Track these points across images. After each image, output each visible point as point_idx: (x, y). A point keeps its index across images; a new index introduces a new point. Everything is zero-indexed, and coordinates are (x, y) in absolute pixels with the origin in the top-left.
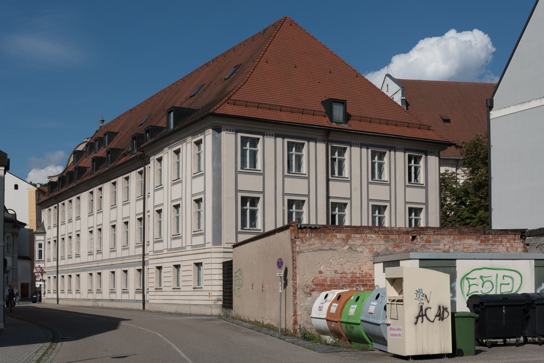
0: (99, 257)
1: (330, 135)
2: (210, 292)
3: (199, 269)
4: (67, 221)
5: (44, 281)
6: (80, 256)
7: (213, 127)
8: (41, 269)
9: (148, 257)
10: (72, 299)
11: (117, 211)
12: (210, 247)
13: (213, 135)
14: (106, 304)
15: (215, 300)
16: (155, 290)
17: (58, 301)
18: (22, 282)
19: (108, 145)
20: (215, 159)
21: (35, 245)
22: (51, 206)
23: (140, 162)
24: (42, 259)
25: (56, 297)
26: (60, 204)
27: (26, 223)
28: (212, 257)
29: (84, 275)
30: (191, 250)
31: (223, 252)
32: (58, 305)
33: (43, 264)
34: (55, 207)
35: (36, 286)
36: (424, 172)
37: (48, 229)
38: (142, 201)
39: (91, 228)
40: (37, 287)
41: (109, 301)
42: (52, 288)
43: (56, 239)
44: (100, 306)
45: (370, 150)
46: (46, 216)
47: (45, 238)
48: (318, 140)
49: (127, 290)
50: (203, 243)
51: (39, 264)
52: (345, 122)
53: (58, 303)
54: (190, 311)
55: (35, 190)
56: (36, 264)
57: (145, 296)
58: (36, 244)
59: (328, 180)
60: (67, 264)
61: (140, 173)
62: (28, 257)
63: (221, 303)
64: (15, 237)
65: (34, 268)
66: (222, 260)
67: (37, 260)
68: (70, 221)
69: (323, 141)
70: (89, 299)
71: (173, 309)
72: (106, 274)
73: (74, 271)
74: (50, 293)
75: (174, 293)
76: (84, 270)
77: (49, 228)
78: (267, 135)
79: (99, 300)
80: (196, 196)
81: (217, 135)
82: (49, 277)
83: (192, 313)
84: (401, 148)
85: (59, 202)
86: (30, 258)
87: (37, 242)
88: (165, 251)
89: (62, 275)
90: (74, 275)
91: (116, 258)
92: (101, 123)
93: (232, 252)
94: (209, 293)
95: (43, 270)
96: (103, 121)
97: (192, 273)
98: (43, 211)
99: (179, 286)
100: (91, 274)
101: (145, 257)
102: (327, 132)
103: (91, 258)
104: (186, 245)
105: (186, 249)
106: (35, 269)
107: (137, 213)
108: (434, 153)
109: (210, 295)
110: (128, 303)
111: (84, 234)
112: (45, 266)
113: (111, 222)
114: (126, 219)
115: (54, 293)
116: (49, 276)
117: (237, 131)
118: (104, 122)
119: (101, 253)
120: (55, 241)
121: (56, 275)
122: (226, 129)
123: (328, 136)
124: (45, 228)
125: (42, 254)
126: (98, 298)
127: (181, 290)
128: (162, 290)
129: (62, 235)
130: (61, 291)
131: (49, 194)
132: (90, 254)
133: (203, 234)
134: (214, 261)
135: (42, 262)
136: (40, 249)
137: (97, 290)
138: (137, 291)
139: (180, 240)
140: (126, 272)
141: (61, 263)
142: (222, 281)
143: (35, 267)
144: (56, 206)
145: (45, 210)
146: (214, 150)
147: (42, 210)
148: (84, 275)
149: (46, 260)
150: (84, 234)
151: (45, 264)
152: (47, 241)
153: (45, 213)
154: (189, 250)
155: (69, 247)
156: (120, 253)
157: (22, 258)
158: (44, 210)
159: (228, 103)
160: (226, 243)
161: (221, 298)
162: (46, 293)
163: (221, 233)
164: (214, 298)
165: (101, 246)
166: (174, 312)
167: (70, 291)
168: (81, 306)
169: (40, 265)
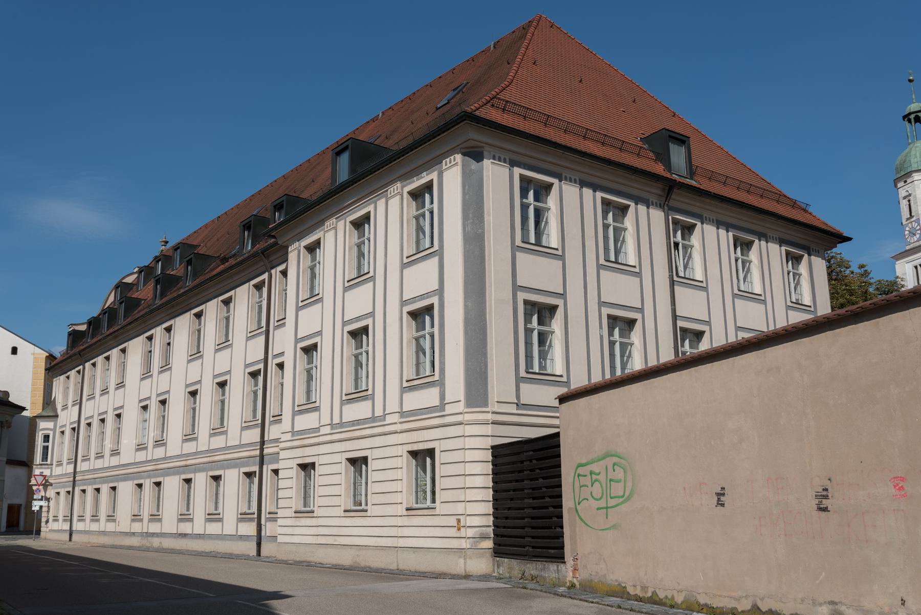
0: (159, 453)
1: (673, 197)
2: (462, 518)
3: (308, 476)
4: (98, 392)
5: (48, 500)
6: (119, 453)
7: (463, 151)
8: (45, 478)
11: (202, 363)
13: (464, 166)
14: (168, 543)
16: (294, 515)
17: (71, 535)
18: (10, 502)
19: (180, 265)
20: (471, 215)
21: (37, 437)
22: (71, 370)
23: (262, 264)
24: (47, 461)
26: (88, 365)
27: (24, 406)
28: (466, 435)
29: (126, 489)
30: (401, 423)
31: (492, 423)
32: (70, 543)
33: (50, 470)
34: (79, 372)
35: (33, 509)
36: (809, 283)
37: (63, 410)
38: (263, 338)
39: (146, 400)
40: (34, 510)
41: (175, 537)
42: (62, 511)
43: (76, 425)
44: (157, 546)
45: (731, 234)
46: (61, 389)
47: (55, 426)
48: (651, 204)
51: (42, 471)
52: (691, 177)
53: (70, 540)
54: (396, 564)
55: (45, 357)
56: (36, 470)
57: (263, 527)
58: (38, 436)
59: (672, 283)
61: (259, 287)
62: (24, 462)
63: (489, 544)
64: (6, 428)
65: (31, 478)
66: (490, 442)
67: (38, 463)
68: (105, 392)
69: (658, 205)
70: (134, 533)
71: (346, 558)
72: (172, 484)
73: (105, 480)
74: (57, 520)
75: (348, 522)
76: (126, 478)
77: (65, 407)
78: (566, 180)
79: (153, 535)
80: (415, 302)
81: (473, 165)
82: (58, 493)
83: (401, 567)
84: (775, 236)
85: (87, 362)
86: (27, 464)
87: (41, 433)
88: (327, 430)
90: (105, 489)
91: (197, 453)
92: (162, 245)
93: (557, 417)
94: (459, 521)
95: (47, 481)
96: (167, 242)
97: (402, 474)
98: (56, 381)
100: (140, 486)
101: (264, 447)
102: (667, 188)
103: (141, 456)
104: (384, 410)
106: (33, 479)
108: (819, 253)
110: (219, 542)
111: (131, 415)
112: (51, 473)
113: (187, 386)
115: (65, 521)
116: (57, 491)
117: (513, 164)
118: (167, 245)
119: (164, 445)
120: (74, 429)
121: (70, 489)
122: (492, 155)
123: (669, 198)
125: (47, 455)
126: (151, 531)
127: (369, 514)
128: (315, 515)
129: (86, 419)
130: (78, 518)
131: (69, 352)
132: (141, 447)
133: (441, 383)
134: (470, 443)
136: (46, 444)
137: (151, 515)
138: (243, 517)
139: (368, 403)
141: (82, 466)
142: (491, 492)
143: (34, 475)
144: (80, 370)
145: (59, 379)
146: (467, 197)
147: (54, 380)
148: (126, 489)
149: (55, 463)
150: (131, 415)
151: (51, 471)
152: (58, 431)
153: (59, 383)
154: (396, 423)
155: (100, 437)
156: (204, 441)
157: (12, 462)
158: (58, 378)
159: (493, 106)
160: (498, 402)
161: (490, 531)
162: (50, 520)
163: (486, 379)
164: (470, 533)
165: (163, 432)
166: (348, 564)
167: (95, 518)
168: (116, 545)
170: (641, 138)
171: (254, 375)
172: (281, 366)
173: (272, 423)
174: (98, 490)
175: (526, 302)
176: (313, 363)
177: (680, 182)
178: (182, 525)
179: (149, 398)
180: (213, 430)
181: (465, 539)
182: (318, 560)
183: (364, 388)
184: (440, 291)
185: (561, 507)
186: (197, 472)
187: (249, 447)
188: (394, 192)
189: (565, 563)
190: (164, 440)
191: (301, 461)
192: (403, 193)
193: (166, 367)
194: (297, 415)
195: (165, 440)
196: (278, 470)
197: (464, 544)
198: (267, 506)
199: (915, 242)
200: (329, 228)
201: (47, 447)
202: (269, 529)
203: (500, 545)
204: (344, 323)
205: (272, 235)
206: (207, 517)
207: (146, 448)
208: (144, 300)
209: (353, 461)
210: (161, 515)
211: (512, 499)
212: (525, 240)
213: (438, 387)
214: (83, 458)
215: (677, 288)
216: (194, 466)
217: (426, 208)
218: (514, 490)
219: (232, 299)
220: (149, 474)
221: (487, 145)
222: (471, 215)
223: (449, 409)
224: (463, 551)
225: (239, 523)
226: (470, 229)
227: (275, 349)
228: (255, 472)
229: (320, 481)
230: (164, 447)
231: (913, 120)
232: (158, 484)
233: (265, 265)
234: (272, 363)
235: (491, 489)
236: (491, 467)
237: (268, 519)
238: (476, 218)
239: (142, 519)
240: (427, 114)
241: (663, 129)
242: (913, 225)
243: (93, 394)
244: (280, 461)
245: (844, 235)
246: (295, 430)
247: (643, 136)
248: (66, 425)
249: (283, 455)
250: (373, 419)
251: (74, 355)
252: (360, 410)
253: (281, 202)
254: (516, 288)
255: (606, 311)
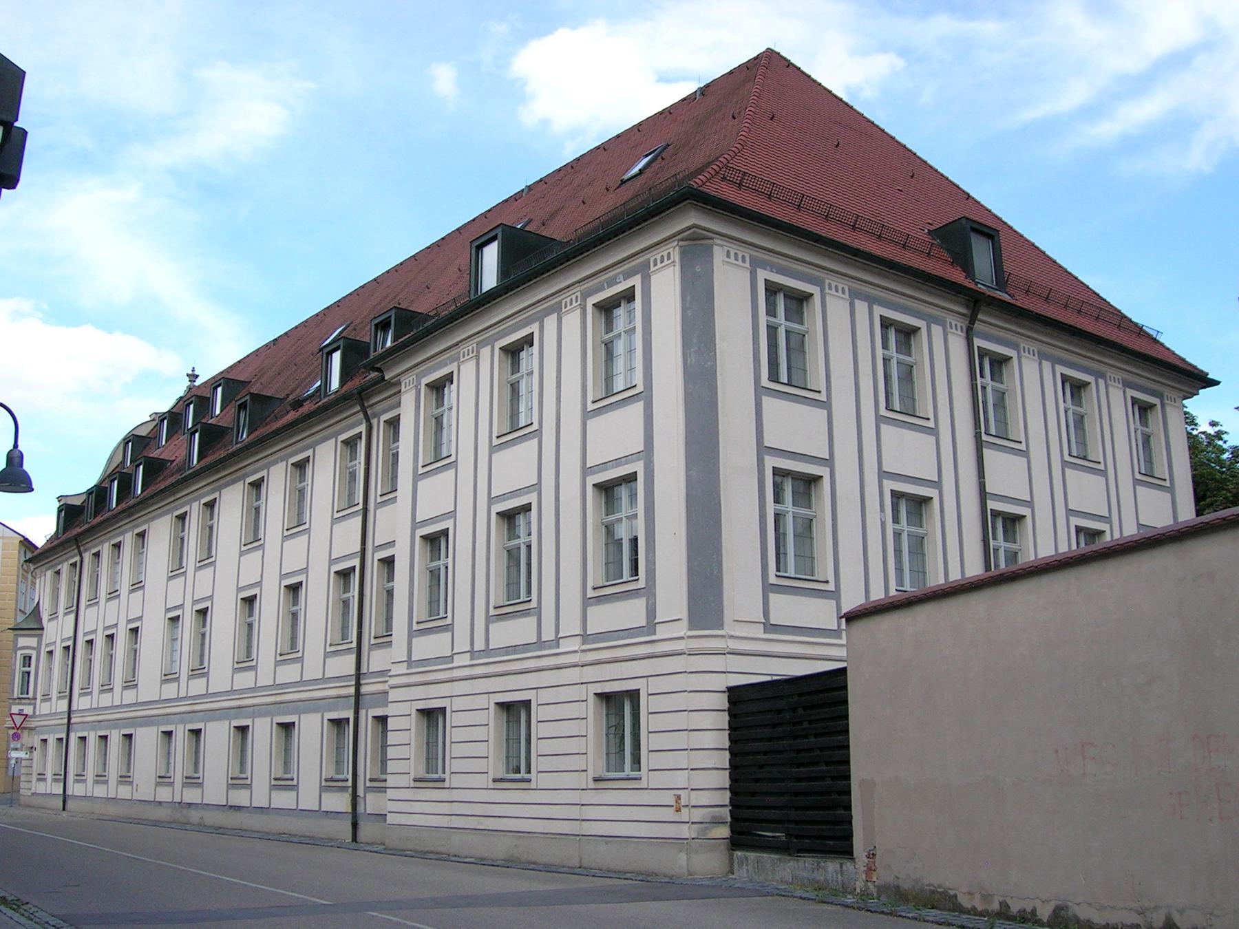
0: (198, 687)
4: (124, 588)
9: (387, 682)
10: (108, 799)
11: (263, 557)
12: (682, 634)
14: (212, 818)
15: (702, 823)
16: (491, 785)
20: (695, 340)
25: (61, 792)
32: (64, 814)
33: (32, 707)
37: (50, 620)
43: (70, 643)
46: (48, 590)
47: (39, 643)
49: (130, 777)
50: (644, 625)
51: (21, 707)
60: (96, 706)
63: (724, 832)
68: (114, 595)
70: (160, 803)
76: (148, 721)
77: (54, 616)
82: (45, 741)
87: (19, 653)
89: (42, 738)
90: (115, 738)
99: (245, 773)
100: (168, 734)
103: (170, 691)
105: (453, 662)
107: (129, 619)
109: (683, 802)
112: (34, 712)
113: (168, 610)
114: (134, 622)
115: (55, 780)
118: (197, 380)
120: (67, 648)
121: (64, 736)
124: (41, 619)
126: (187, 800)
128: (446, 784)
129: (86, 634)
130: (76, 778)
133: (649, 592)
135: (27, 701)
136: (27, 669)
138: (330, 785)
139: (531, 621)
140: (287, 727)
141: (81, 703)
142: (727, 755)
146: (689, 313)
149: (39, 696)
151: (35, 708)
159: (724, 179)
161: (726, 813)
164: (698, 815)
167: (101, 779)
169: (23, 710)
170: (929, 230)
171: (345, 575)
172: (389, 562)
173: (372, 647)
174: (105, 738)
175: (777, 472)
176: (440, 559)
177: (989, 296)
178: (233, 793)
179: (181, 606)
180: (237, 663)
181: (688, 825)
182: (453, 851)
183: (523, 598)
184: (647, 453)
185: (848, 777)
186: (255, 717)
187: (337, 682)
188: (571, 304)
189: (853, 859)
190: (205, 668)
191: (422, 705)
192: (585, 306)
193: (207, 558)
194: (494, 622)
195: (255, 661)
196: (387, 716)
197: (685, 832)
198: (367, 769)
200: (466, 358)
201: (29, 673)
202: (371, 803)
203: (741, 833)
204: (491, 500)
205: (377, 368)
206: (273, 782)
207: (177, 680)
208: (170, 461)
209: (506, 707)
210: (201, 778)
211: (762, 767)
213: (645, 599)
214: (81, 691)
216: (252, 708)
218: (766, 753)
219: (308, 461)
220: (182, 717)
222: (695, 340)
223: (661, 633)
224: (686, 842)
225: (323, 794)
226: (693, 360)
227: (380, 534)
228: (348, 719)
229: (453, 735)
230: (205, 679)
232: (197, 733)
234: (373, 558)
235: (728, 752)
236: (727, 718)
237: (367, 789)
238: (703, 345)
239: (173, 782)
240: (608, 190)
243: (96, 598)
244: (390, 704)
246: (413, 659)
247: (932, 228)
248: (55, 642)
249: (394, 695)
250: (540, 644)
251: (68, 541)
252: (519, 631)
253: (387, 318)
254: (763, 450)
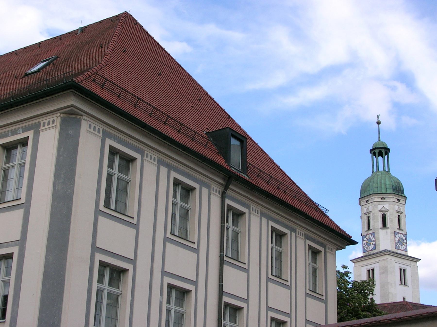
1: (230, 187)
20: (62, 176)
102: (227, 179)
146: (61, 158)
159: (94, 80)
170: (206, 132)
199: (370, 251)
212: (107, 205)
215: (225, 267)
217: (17, 162)
221: (85, 115)
222: (62, 176)
231: (377, 154)
233: (368, 239)
240: (16, 78)
241: (227, 128)
242: (370, 237)
245: (352, 239)
254: (95, 249)
255: (168, 280)
